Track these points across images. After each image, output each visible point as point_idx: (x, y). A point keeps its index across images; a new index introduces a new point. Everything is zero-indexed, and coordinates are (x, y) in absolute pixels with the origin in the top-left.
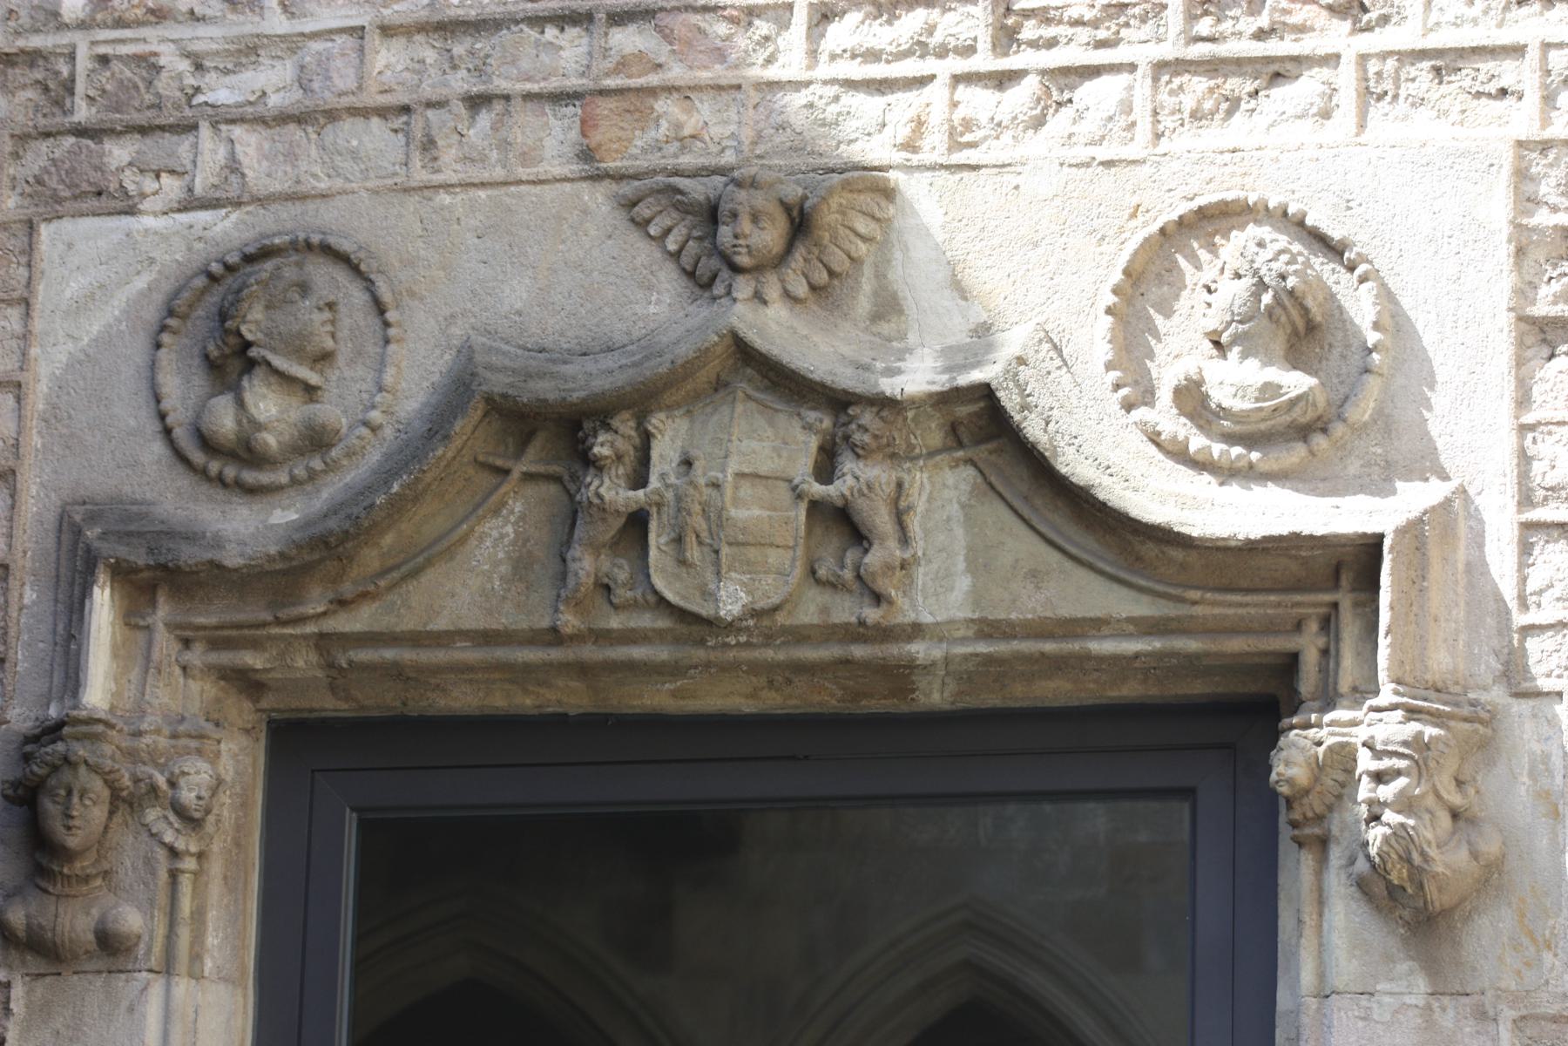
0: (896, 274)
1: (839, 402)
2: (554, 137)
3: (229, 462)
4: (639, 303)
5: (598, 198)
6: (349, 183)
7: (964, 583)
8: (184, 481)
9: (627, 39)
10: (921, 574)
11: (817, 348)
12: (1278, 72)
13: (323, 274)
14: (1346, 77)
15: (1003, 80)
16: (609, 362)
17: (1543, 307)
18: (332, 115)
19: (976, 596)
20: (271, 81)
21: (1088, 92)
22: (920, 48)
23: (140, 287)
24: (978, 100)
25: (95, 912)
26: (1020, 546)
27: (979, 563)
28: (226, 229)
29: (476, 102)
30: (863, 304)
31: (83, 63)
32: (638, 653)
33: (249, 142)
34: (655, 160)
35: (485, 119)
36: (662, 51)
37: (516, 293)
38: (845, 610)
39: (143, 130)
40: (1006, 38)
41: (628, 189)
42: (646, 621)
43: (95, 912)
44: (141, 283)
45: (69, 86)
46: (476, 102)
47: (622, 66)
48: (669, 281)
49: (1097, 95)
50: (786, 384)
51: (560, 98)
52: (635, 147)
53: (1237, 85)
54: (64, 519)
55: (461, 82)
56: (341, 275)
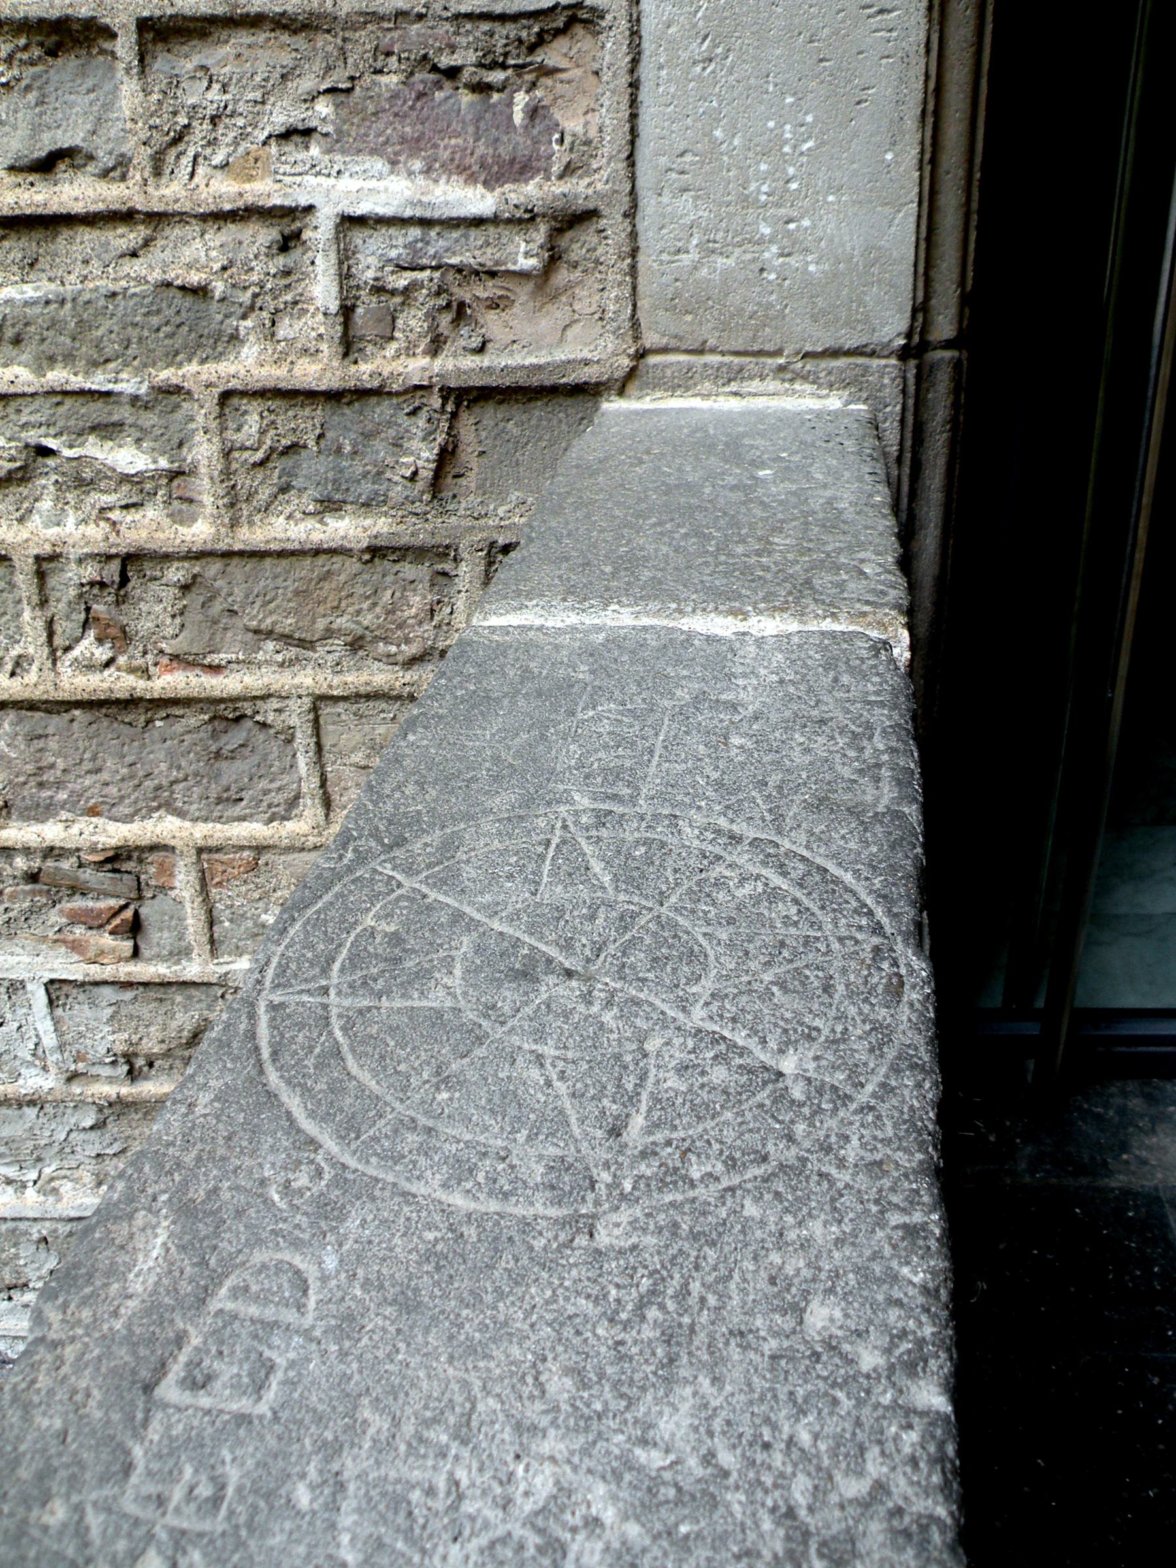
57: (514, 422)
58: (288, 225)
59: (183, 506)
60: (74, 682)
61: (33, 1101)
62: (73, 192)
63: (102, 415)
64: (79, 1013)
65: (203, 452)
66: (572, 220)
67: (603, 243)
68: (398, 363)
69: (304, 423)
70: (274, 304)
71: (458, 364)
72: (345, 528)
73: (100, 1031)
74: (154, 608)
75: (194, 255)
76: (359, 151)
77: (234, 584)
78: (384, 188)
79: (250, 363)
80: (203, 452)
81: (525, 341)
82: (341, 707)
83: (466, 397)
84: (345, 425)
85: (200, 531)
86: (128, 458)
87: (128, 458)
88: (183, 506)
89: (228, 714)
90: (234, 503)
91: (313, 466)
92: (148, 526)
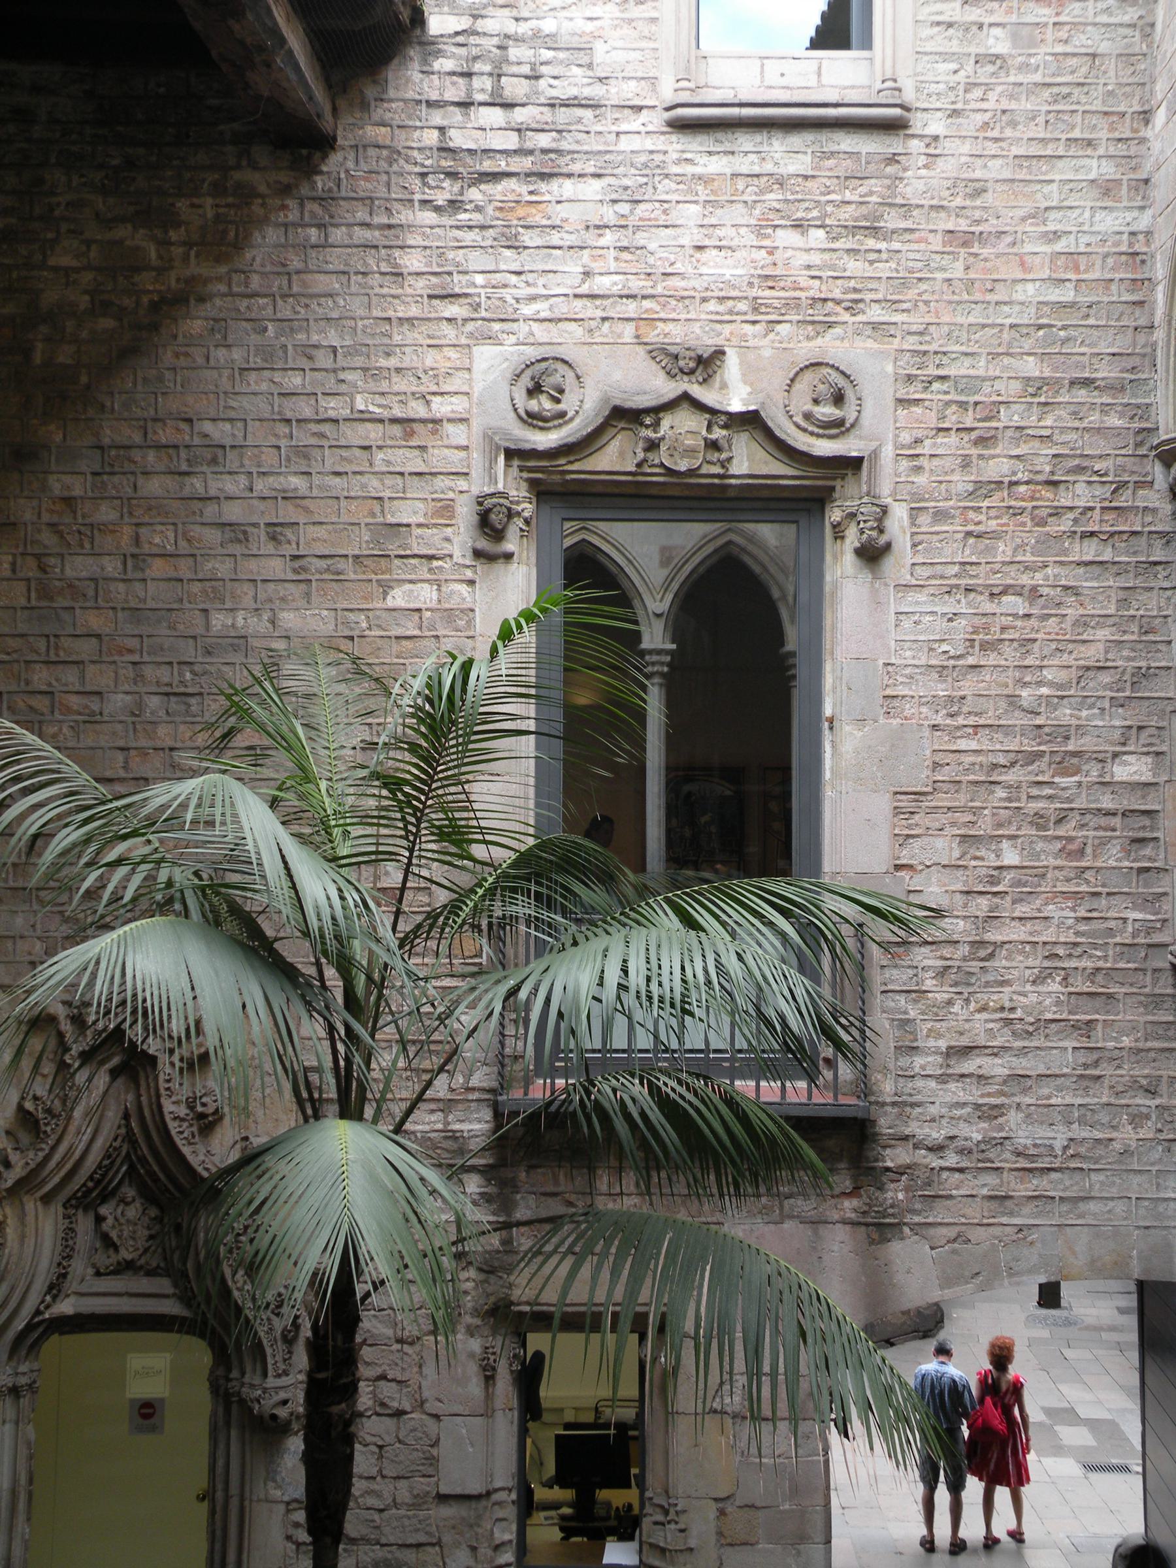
0: (726, 376)
1: (713, 412)
2: (629, 330)
3: (533, 419)
4: (665, 388)
5: (641, 350)
6: (567, 339)
7: (746, 464)
8: (520, 425)
9: (647, 304)
10: (735, 461)
11: (708, 396)
12: (830, 325)
13: (560, 366)
14: (850, 330)
15: (754, 322)
16: (646, 397)
17: (899, 396)
18: (560, 320)
19: (749, 467)
20: (541, 308)
21: (779, 327)
22: (731, 312)
23: (506, 369)
24: (748, 328)
25: (948, 1293)
26: (761, 454)
27: (751, 459)
28: (532, 353)
29: (604, 319)
30: (717, 385)
31: (483, 299)
32: (654, 479)
33: (535, 326)
34: (656, 340)
35: (607, 324)
36: (658, 308)
37: (617, 376)
38: (717, 470)
39: (503, 320)
40: (755, 310)
41: (649, 348)
42: (657, 470)
43: (948, 1293)
44: (505, 365)
45: (479, 305)
46: (604, 319)
47: (646, 311)
48: (662, 375)
49: (783, 329)
50: (699, 406)
51: (628, 319)
52: (653, 335)
53: (819, 327)
54: (485, 435)
55: (599, 313)
56: (566, 367)
57: (1156, 950)
58: (1125, 920)
59: (1106, 961)
60: (1086, 990)
61: (1064, 1075)
62: (1095, 914)
63: (1095, 946)
64: (1077, 1053)
65: (1111, 953)
66: (1165, 921)
67: (1169, 924)
68: (1141, 940)
69: (1126, 949)
70: (1123, 931)
71: (1147, 941)
72: (1130, 965)
73: (1082, 1058)
74: (1099, 978)
75: (1112, 924)
76: (1042, 1123)
77: (1113, 973)
78: (1140, 916)
79: (1118, 940)
80: (1111, 953)
81: (1157, 938)
82: (523, 1229)
83: (1150, 946)
84: (1132, 950)
85: (1109, 965)
86: (1099, 953)
87: (1099, 953)
88: (1106, 961)
89: (1110, 996)
90: (1115, 961)
91: (1126, 956)
92: (1101, 964)
